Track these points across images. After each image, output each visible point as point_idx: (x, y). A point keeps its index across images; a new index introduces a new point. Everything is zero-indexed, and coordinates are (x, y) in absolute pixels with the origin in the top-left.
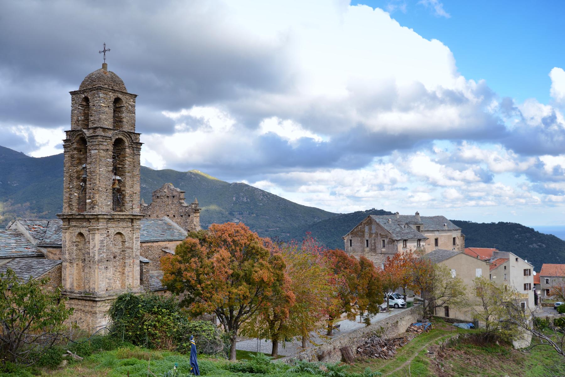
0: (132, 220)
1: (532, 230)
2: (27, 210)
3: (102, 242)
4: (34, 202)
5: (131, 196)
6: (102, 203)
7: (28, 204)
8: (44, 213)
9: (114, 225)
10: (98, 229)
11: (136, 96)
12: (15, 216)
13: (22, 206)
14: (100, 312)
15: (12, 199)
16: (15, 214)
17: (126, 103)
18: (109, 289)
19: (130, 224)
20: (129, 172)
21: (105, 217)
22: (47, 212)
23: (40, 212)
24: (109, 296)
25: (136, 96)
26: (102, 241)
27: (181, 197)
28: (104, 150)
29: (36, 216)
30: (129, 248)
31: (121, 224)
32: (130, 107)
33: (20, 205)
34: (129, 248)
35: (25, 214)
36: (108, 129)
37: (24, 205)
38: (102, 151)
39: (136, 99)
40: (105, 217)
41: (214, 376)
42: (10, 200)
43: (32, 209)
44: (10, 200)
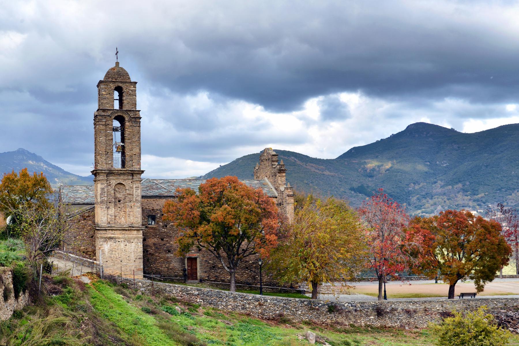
0: (132, 175)
1: (5, 153)
2: (459, 192)
3: (103, 189)
4: (468, 183)
5: (131, 156)
6: (102, 162)
7: (460, 185)
8: (480, 196)
9: (114, 178)
10: (99, 180)
11: (136, 83)
12: (445, 199)
13: (453, 187)
14: (102, 238)
15: (441, 180)
16: (445, 198)
17: (127, 89)
18: (111, 222)
19: (131, 178)
20: (129, 139)
21: (103, 171)
22: (483, 195)
23: (474, 194)
24: (109, 227)
25: (136, 83)
26: (103, 188)
27: (274, 159)
28: (103, 125)
29: (470, 200)
30: (130, 195)
31: (122, 177)
32: (130, 92)
33: (450, 187)
34: (130, 195)
35: (456, 197)
36: (108, 110)
37: (455, 187)
38: (101, 126)
39: (137, 85)
40: (103, 171)
41: (399, 344)
42: (439, 182)
43: (465, 191)
44: (439, 182)
